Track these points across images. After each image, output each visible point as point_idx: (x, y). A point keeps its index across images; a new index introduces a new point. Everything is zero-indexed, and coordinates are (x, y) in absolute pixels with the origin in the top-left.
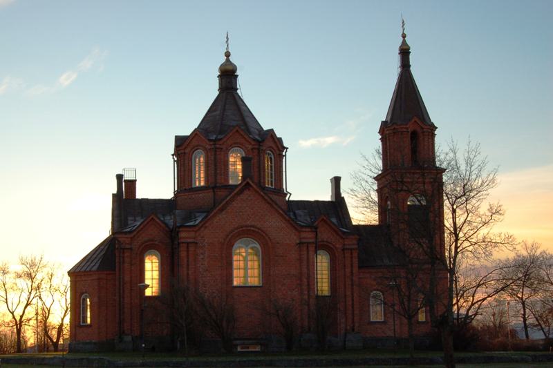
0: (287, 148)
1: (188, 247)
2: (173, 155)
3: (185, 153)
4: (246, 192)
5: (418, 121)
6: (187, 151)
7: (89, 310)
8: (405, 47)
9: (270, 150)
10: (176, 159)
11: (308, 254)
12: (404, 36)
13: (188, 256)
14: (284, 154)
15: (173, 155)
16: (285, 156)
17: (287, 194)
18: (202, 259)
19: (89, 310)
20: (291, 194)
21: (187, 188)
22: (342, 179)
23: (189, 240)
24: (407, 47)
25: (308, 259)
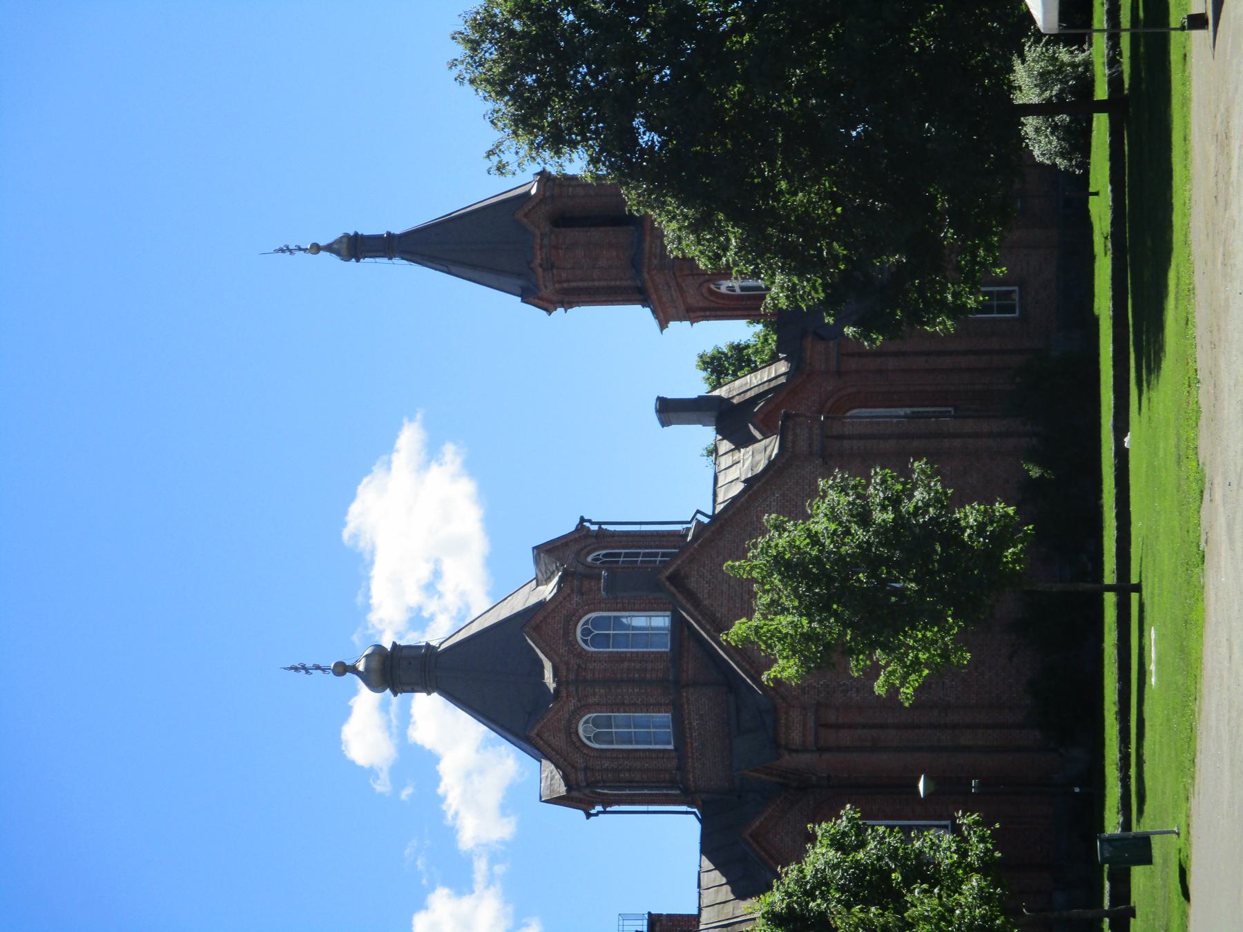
0: (582, 520)
1: (827, 726)
2: (589, 815)
3: (586, 768)
4: (692, 583)
5: (526, 210)
6: (580, 763)
7: (1126, 153)
8: (344, 246)
9: (588, 554)
10: (599, 808)
11: (849, 437)
12: (316, 248)
13: (850, 726)
14: (595, 528)
15: (589, 815)
16: (600, 524)
17: (699, 522)
18: (858, 691)
19: (1126, 153)
20: (698, 512)
21: (675, 762)
22: (660, 427)
23: (811, 723)
24: (345, 240)
25: (861, 437)
